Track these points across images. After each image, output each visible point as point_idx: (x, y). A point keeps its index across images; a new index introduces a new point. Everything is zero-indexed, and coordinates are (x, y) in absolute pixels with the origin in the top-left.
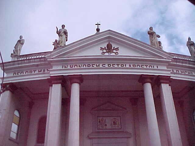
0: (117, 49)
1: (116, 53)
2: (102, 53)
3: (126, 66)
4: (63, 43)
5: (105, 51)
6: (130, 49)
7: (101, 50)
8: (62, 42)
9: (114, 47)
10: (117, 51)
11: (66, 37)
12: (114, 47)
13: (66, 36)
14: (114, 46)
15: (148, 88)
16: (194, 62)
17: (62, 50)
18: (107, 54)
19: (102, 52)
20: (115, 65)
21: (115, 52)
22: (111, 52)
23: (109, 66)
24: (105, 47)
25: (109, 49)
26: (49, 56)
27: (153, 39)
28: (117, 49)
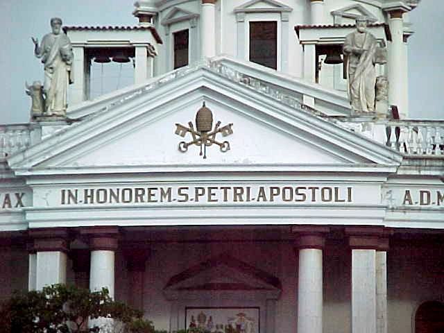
0: (227, 130)
1: (222, 145)
2: (180, 148)
3: (262, 189)
4: (59, 98)
5: (189, 138)
6: (330, 108)
7: (177, 133)
8: (55, 95)
9: (219, 123)
10: (225, 135)
11: (69, 72)
12: (219, 123)
13: (69, 69)
14: (220, 116)
15: (311, 262)
16: (443, 166)
17: (58, 143)
18: (194, 149)
19: (383, 40)
20: (305, 188)
21: (221, 142)
22: (208, 142)
23: (278, 194)
24: (190, 124)
25: (203, 132)
26: (19, 163)
27: (356, 75)
28: (227, 130)
